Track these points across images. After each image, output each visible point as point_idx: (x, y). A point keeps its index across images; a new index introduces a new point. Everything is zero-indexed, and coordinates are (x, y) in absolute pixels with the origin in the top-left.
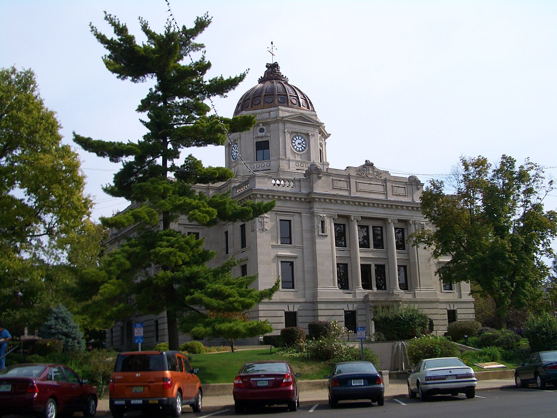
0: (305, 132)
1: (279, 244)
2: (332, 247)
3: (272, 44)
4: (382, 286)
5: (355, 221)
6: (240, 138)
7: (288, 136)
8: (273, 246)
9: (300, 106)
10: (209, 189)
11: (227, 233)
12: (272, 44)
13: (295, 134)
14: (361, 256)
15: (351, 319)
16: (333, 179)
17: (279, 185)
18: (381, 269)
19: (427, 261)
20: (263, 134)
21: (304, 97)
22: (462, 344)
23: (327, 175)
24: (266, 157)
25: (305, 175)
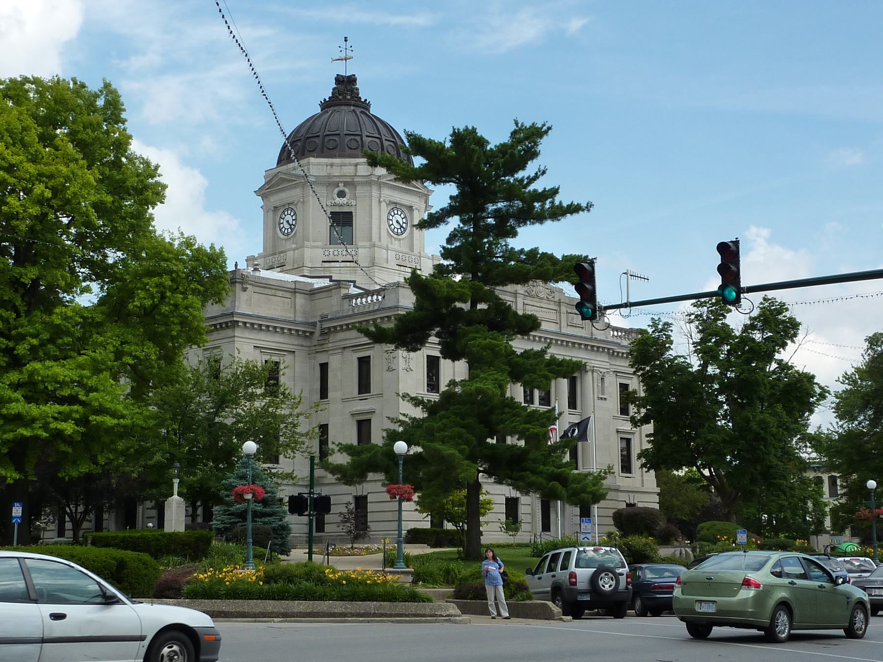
0: (408, 203)
3: (346, 41)
6: (303, 202)
7: (385, 209)
10: (295, 293)
12: (346, 41)
13: (395, 206)
20: (344, 200)
22: (471, 599)
24: (349, 240)
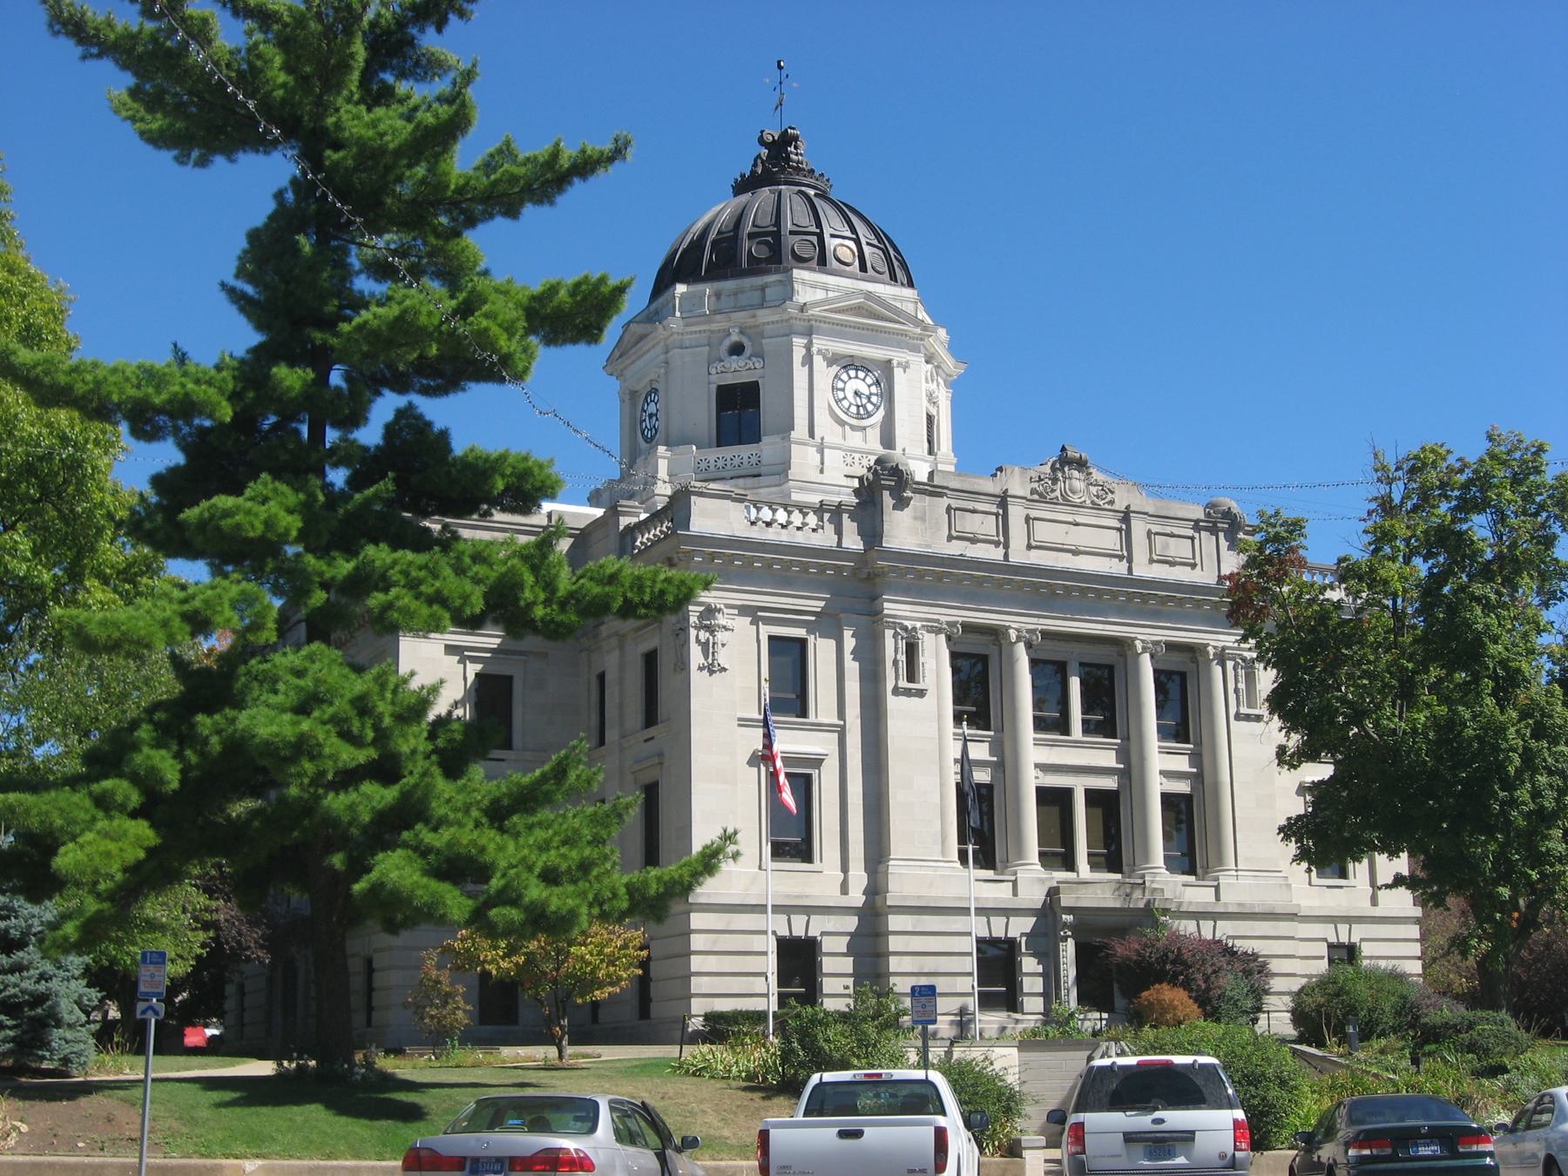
2: (940, 729)
4: (1111, 856)
11: (602, 678)
14: (1039, 759)
15: (998, 968)
16: (949, 509)
17: (768, 524)
18: (1110, 809)
19: (1263, 777)
23: (932, 494)
25: (857, 492)
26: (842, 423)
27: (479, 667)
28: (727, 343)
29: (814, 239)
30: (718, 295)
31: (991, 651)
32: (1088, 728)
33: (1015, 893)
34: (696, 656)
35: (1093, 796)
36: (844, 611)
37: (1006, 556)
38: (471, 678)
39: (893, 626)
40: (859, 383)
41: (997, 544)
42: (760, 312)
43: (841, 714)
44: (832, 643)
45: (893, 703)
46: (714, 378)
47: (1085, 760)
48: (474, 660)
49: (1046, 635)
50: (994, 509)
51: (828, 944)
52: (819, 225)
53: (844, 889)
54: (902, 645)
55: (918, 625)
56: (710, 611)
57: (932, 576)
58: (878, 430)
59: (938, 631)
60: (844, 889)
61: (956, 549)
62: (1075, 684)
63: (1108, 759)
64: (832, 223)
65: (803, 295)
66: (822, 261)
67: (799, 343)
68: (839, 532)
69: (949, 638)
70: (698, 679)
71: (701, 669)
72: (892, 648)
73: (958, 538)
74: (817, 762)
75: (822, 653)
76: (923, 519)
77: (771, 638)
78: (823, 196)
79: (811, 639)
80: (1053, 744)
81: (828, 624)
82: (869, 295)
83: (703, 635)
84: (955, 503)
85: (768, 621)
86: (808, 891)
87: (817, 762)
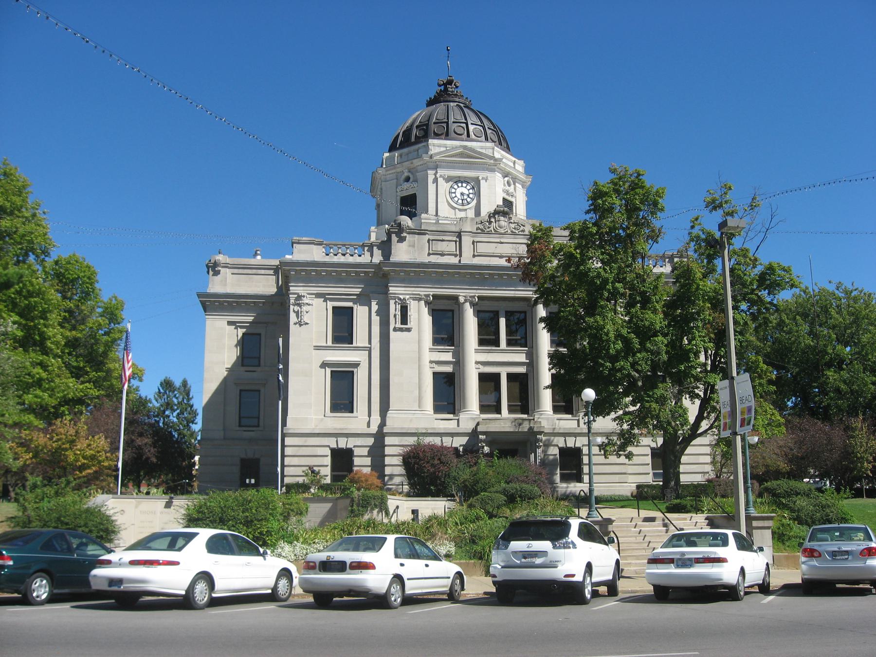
1: (330, 343)
5: (467, 305)
8: (317, 348)
9: (468, 135)
14: (476, 359)
21: (494, 127)
23: (419, 234)
26: (454, 208)
27: (244, 330)
28: (403, 177)
29: (464, 125)
30: (401, 156)
31: (455, 308)
32: (510, 343)
33: (458, 425)
34: (293, 318)
35: (511, 377)
36: (373, 292)
37: (460, 261)
38: (240, 335)
39: (394, 298)
40: (464, 189)
41: (456, 255)
42: (415, 161)
43: (370, 342)
44: (367, 308)
45: (393, 335)
46: (399, 194)
47: (508, 359)
48: (241, 327)
49: (480, 298)
50: (455, 238)
51: (357, 451)
52: (466, 119)
53: (369, 426)
54: (398, 307)
55: (408, 297)
56: (299, 297)
57: (415, 273)
58: (473, 211)
59: (420, 300)
60: (369, 426)
61: (434, 259)
62: (503, 322)
63: (522, 358)
64: (472, 118)
65: (433, 150)
66: (447, 134)
67: (431, 173)
68: (372, 256)
69: (427, 303)
70: (293, 329)
71: (295, 324)
72: (394, 309)
73: (433, 254)
74: (356, 365)
75: (361, 314)
76: (413, 246)
77: (334, 308)
78: (467, 107)
79: (355, 307)
80: (489, 352)
81: (363, 299)
82: (465, 147)
83: (296, 308)
84: (432, 237)
85: (332, 300)
86: (349, 426)
87: (356, 365)
